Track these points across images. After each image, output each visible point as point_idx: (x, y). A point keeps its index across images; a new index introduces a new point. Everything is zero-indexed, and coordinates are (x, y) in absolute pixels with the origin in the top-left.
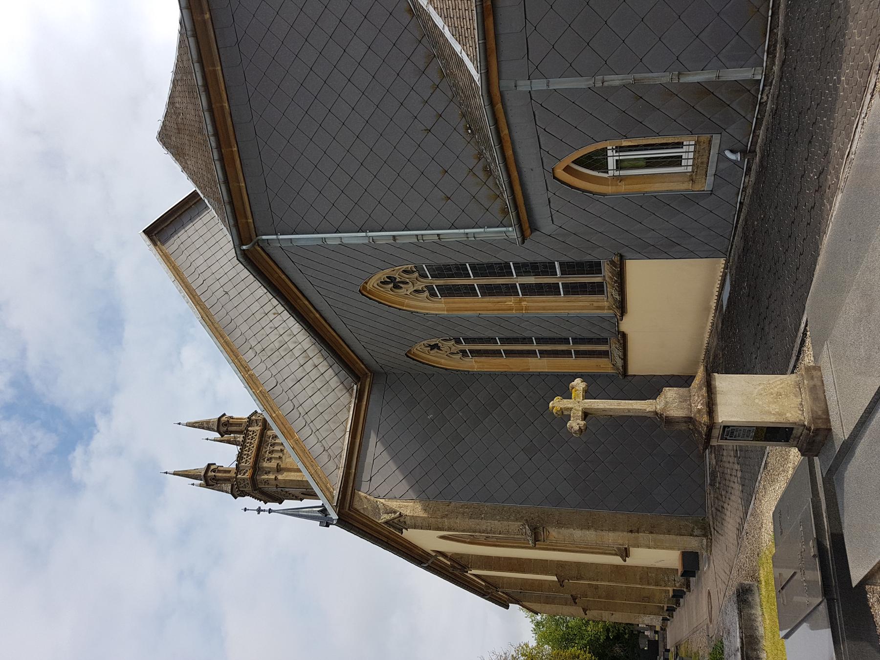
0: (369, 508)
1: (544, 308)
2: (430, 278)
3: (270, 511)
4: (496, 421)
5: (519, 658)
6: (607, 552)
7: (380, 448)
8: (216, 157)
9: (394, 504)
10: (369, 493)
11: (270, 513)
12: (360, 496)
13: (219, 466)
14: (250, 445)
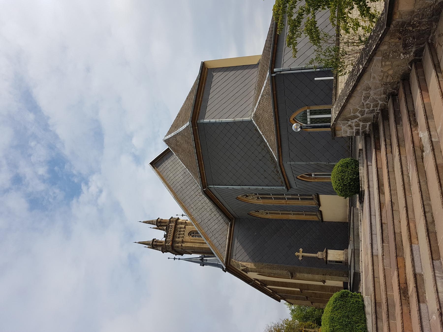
0: (236, 265)
1: (294, 204)
2: (258, 195)
3: (179, 259)
4: (261, 179)
5: (284, 325)
6: (317, 281)
7: (239, 244)
8: (198, 165)
9: (244, 264)
10: (235, 259)
11: (179, 260)
12: (232, 261)
13: (157, 240)
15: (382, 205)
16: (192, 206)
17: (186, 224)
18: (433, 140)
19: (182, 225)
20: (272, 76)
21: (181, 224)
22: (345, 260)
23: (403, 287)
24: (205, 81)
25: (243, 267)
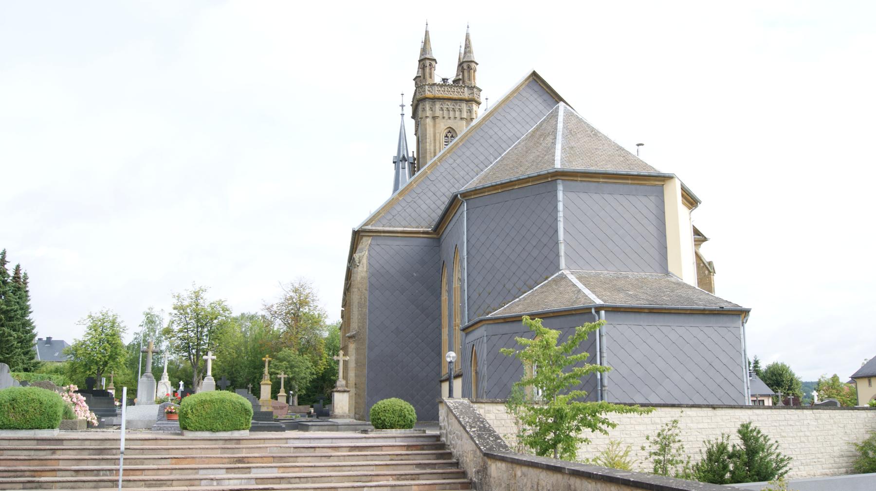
1: (455, 338)
11: (401, 114)
12: (368, 240)
14: (452, 91)
15: (336, 449)
16: (459, 161)
17: (469, 119)
18: (244, 449)
19: (467, 112)
20: (591, 308)
21: (469, 110)
22: (335, 415)
23: (244, 460)
24: (638, 184)
25: (359, 258)
